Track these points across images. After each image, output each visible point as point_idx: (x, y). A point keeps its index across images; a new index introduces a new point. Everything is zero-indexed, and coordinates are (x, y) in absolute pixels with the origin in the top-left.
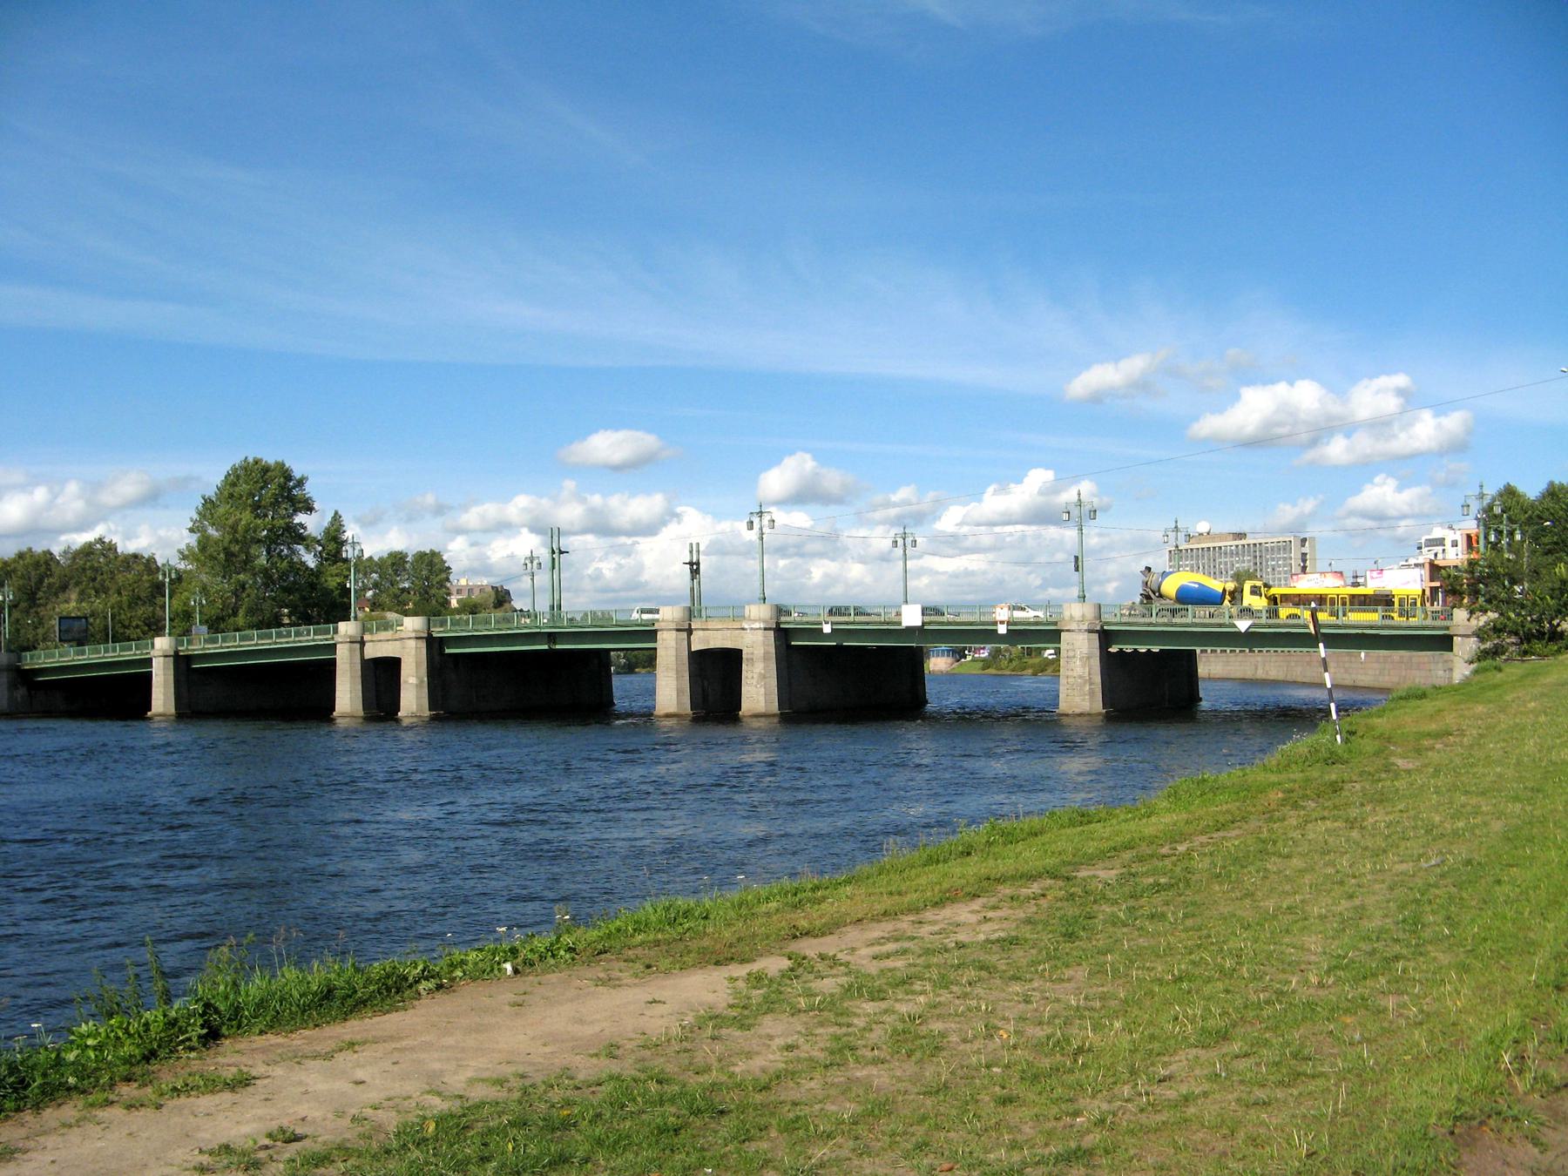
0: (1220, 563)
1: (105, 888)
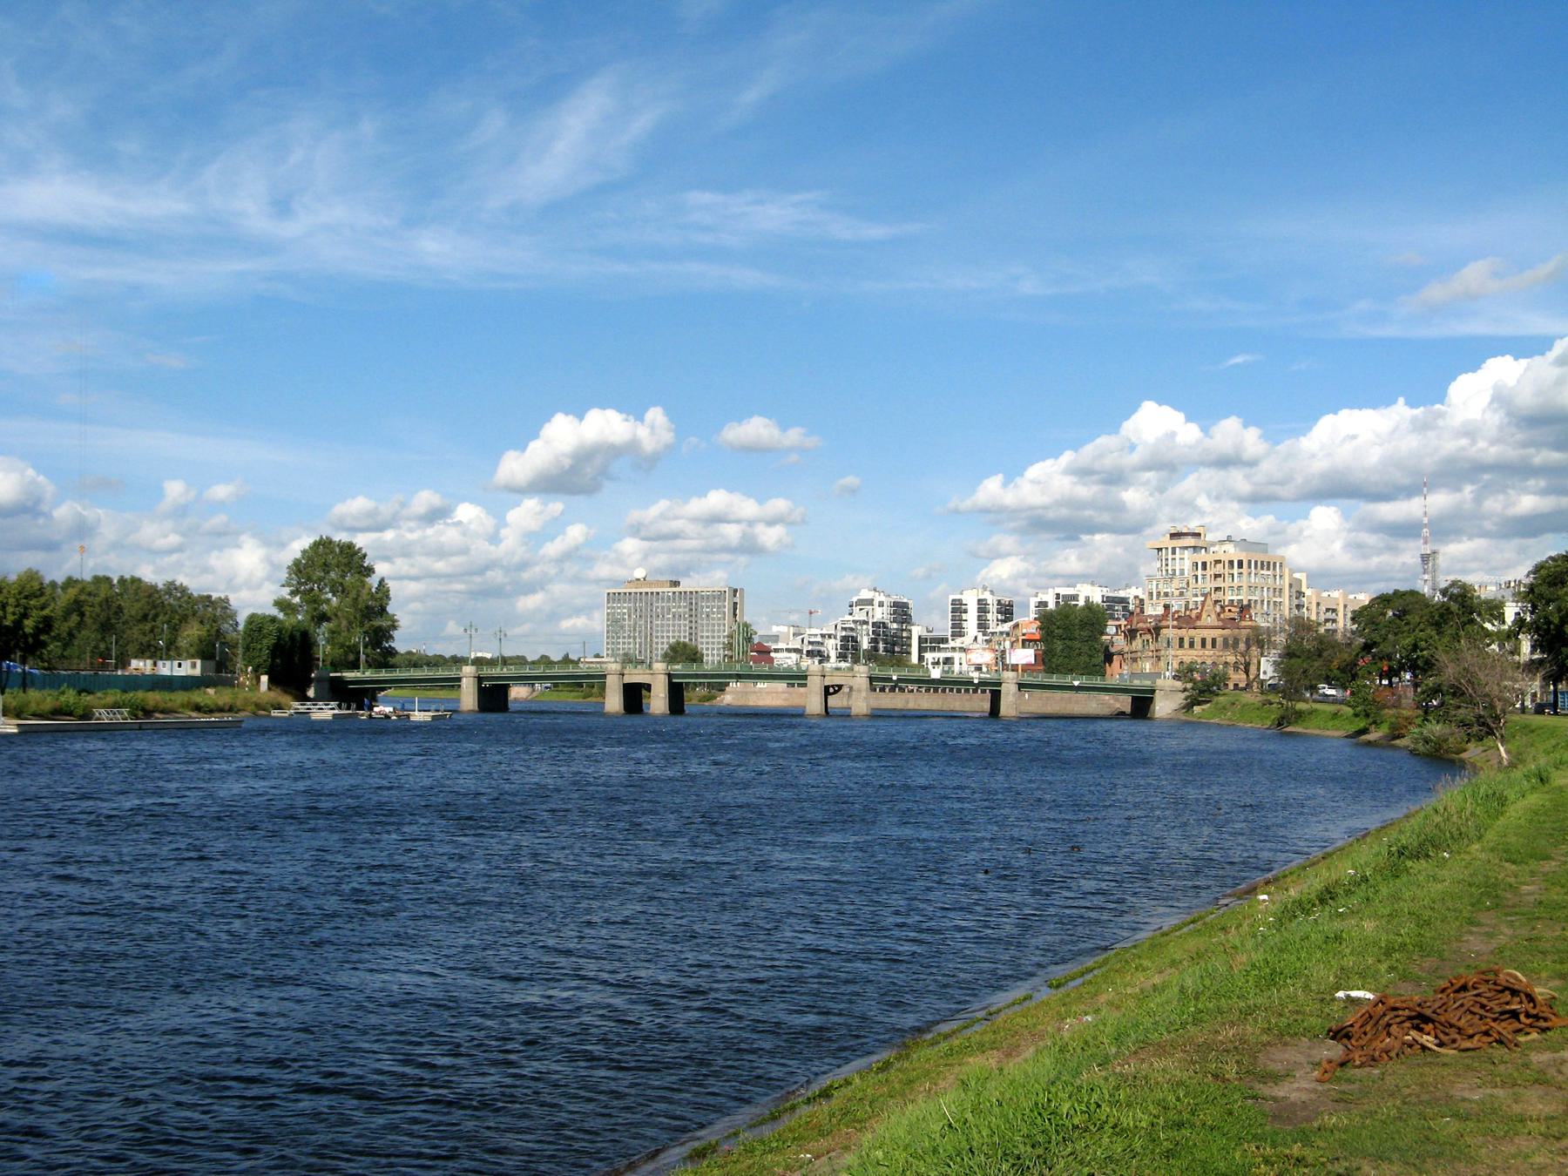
0: (658, 607)
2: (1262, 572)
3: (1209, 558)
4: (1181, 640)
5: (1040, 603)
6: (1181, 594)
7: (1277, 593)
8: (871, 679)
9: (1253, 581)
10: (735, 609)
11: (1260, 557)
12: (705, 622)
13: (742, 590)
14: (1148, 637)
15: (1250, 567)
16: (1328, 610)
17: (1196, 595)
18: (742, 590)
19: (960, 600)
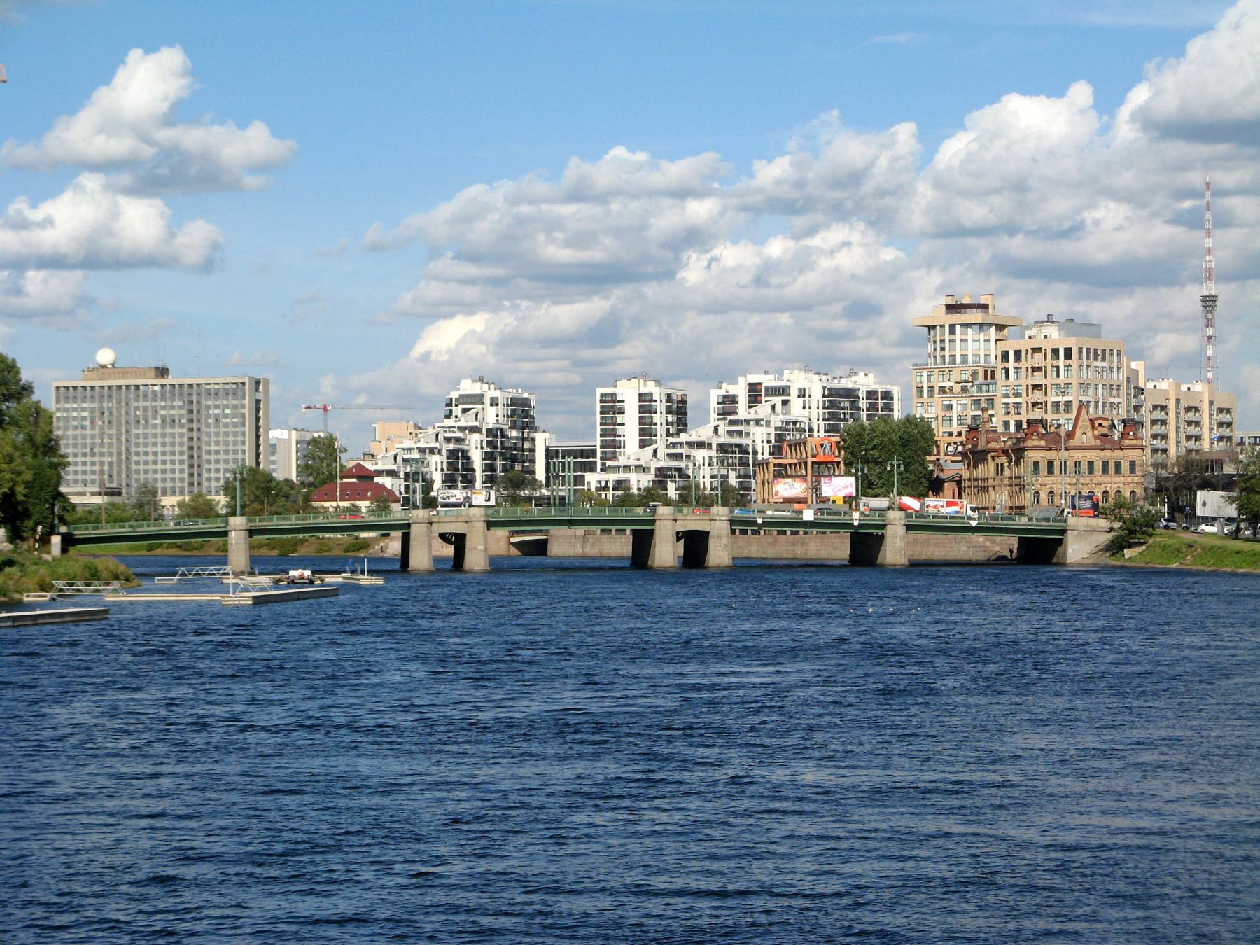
1: (1240, 656)
2: (1096, 364)
3: (1024, 345)
4: (1051, 464)
5: (725, 397)
6: (964, 390)
7: (1115, 392)
8: (733, 522)
9: (1085, 377)
10: (258, 409)
11: (1093, 344)
12: (213, 430)
13: (267, 381)
14: (1004, 460)
15: (1080, 357)
16: (1155, 407)
17: (1007, 396)
18: (267, 381)
19: (614, 395)
